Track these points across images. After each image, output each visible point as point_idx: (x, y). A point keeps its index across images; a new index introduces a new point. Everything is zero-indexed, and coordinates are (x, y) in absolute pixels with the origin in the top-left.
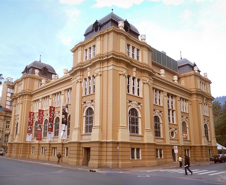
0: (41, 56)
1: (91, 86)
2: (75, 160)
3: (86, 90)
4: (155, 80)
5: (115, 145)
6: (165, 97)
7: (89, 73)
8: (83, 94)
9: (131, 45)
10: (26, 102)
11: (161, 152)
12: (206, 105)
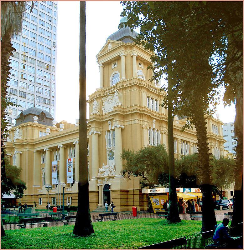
1: (72, 152)
2: (119, 208)
3: (71, 154)
7: (110, 126)
8: (107, 146)
10: (27, 152)
12: (157, 131)
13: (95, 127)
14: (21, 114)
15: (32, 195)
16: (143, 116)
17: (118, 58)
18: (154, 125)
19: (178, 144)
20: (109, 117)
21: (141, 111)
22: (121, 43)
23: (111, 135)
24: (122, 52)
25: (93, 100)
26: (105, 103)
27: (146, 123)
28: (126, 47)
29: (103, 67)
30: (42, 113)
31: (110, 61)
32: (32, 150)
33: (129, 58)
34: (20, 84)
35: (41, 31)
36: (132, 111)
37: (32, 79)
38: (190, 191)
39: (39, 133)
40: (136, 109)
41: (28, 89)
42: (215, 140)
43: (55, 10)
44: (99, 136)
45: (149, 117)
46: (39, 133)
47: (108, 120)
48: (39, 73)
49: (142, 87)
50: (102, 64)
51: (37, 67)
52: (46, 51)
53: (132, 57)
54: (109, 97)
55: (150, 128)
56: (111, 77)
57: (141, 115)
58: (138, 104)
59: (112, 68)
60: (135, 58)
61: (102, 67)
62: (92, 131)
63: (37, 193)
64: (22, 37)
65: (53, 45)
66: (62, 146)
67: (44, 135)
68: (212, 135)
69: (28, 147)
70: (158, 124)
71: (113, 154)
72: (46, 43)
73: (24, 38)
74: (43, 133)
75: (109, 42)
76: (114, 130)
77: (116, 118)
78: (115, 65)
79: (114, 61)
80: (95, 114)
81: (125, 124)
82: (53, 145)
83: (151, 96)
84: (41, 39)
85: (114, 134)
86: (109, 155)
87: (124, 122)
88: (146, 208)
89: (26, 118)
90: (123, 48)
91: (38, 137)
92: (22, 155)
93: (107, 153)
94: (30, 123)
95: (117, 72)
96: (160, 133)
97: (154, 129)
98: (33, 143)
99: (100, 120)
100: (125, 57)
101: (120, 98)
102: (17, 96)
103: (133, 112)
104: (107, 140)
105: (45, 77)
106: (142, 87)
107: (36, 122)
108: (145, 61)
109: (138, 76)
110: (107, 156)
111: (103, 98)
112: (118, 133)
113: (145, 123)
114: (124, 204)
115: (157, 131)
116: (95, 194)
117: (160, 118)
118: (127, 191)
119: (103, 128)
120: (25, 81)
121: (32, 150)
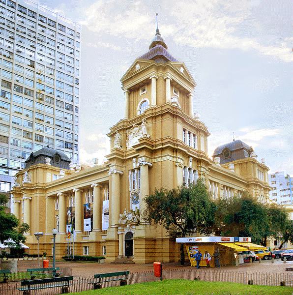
0: (157, 14)
4: (212, 171)
5: (79, 245)
6: (221, 190)
7: (134, 164)
9: (187, 130)
11: (196, 245)
12: (194, 171)
13: (115, 165)
14: (32, 155)
15: (44, 244)
16: (176, 152)
17: (148, 82)
18: (191, 163)
19: (219, 191)
20: (134, 153)
21: (174, 145)
22: (152, 63)
23: (135, 175)
24: (152, 74)
25: (116, 133)
26: (130, 136)
27: (180, 160)
28: (158, 68)
29: (129, 94)
30: (57, 154)
31: (137, 86)
32: (44, 195)
33: (161, 82)
34: (36, 126)
35: (61, 66)
36: (163, 144)
37: (51, 121)
38: (238, 240)
39: (52, 177)
40: (169, 142)
41: (46, 132)
42: (260, 187)
43: (77, 39)
44: (121, 176)
45: (185, 155)
46: (52, 177)
47: (133, 158)
48: (58, 115)
49: (177, 116)
50: (128, 89)
51: (56, 107)
52: (67, 89)
53: (165, 80)
54: (135, 129)
55: (185, 167)
56: (139, 105)
57: (175, 151)
58: (171, 136)
59: (141, 94)
60: (168, 82)
61: (128, 94)
62: (112, 170)
63: (44, 242)
64: (37, 73)
65: (75, 82)
66: (77, 190)
67: (58, 178)
68: (257, 180)
69: (38, 191)
70: (195, 164)
71: (138, 197)
72: (69, 80)
73: (39, 74)
74: (57, 176)
75: (138, 62)
76: (139, 169)
77: (143, 153)
78: (144, 90)
79: (142, 86)
80: (117, 150)
81: (153, 161)
82: (67, 188)
83: (188, 129)
84: (60, 75)
85: (139, 174)
86: (133, 198)
87: (152, 159)
88: (177, 259)
89: (37, 160)
90: (153, 68)
91: (52, 180)
92: (32, 202)
93: (131, 196)
94: (40, 165)
95: (146, 99)
96: (197, 174)
97: (190, 169)
98: (44, 187)
99: (123, 156)
100: (157, 80)
101: (148, 129)
102: (32, 139)
103: (164, 146)
104: (131, 182)
105: (66, 118)
106: (177, 116)
107: (48, 164)
108: (182, 89)
109: (172, 103)
110: (131, 199)
111: (127, 131)
112: (144, 171)
113: (179, 160)
114: (150, 255)
115: (194, 171)
116: (114, 243)
117: (199, 156)
118: (155, 240)
119: (125, 167)
120: (41, 122)
121: (44, 195)
